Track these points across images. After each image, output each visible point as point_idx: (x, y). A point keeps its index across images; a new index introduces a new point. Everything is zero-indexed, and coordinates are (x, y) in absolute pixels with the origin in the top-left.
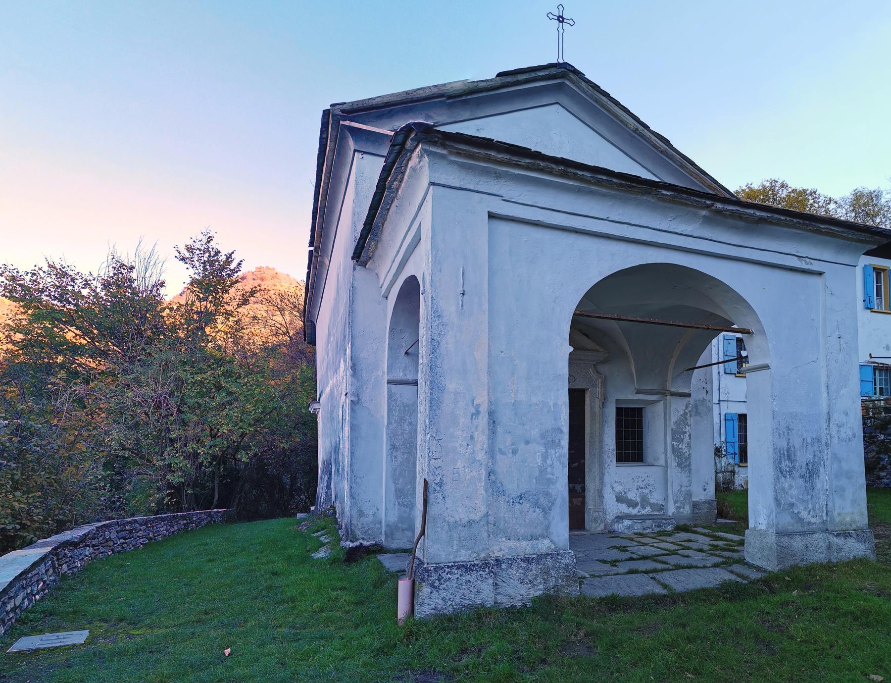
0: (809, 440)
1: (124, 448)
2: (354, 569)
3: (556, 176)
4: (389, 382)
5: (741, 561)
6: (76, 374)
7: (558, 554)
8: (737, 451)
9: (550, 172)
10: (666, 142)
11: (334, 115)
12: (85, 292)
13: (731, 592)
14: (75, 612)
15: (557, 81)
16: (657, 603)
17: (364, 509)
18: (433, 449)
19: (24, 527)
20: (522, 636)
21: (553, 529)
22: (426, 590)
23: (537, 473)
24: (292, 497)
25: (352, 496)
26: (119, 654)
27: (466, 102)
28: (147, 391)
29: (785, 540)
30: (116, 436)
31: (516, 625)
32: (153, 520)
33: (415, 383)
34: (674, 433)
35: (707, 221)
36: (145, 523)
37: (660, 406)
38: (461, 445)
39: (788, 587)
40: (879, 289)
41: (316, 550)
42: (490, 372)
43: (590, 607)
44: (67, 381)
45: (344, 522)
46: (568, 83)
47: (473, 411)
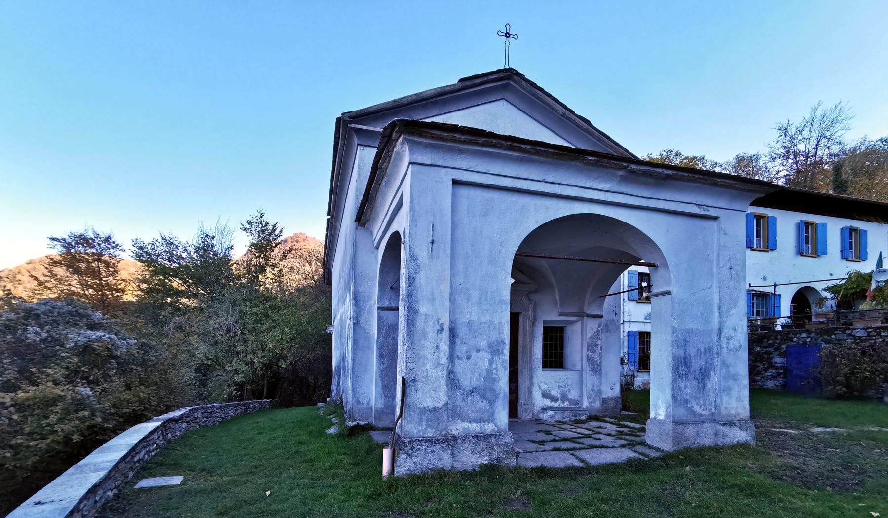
0: (702, 350)
1: (208, 359)
2: (353, 441)
3: (505, 149)
4: (379, 309)
5: (643, 444)
6: (179, 309)
8: (637, 360)
9: (500, 147)
10: (587, 122)
11: (344, 121)
12: (184, 255)
13: (633, 466)
14: (175, 464)
15: (505, 83)
16: (576, 473)
17: (360, 398)
18: (409, 355)
19: (146, 409)
20: (472, 491)
21: (497, 416)
22: (403, 456)
23: (485, 374)
24: (315, 392)
25: (353, 390)
26: (200, 492)
27: (435, 103)
28: (222, 320)
29: (680, 428)
30: (202, 350)
31: (467, 483)
32: (224, 406)
33: (397, 309)
34: (588, 345)
35: (624, 179)
36: (220, 408)
37: (579, 325)
39: (682, 464)
40: (758, 231)
41: (329, 428)
42: (452, 300)
43: (524, 475)
44: (172, 314)
45: (347, 408)
46: (511, 83)
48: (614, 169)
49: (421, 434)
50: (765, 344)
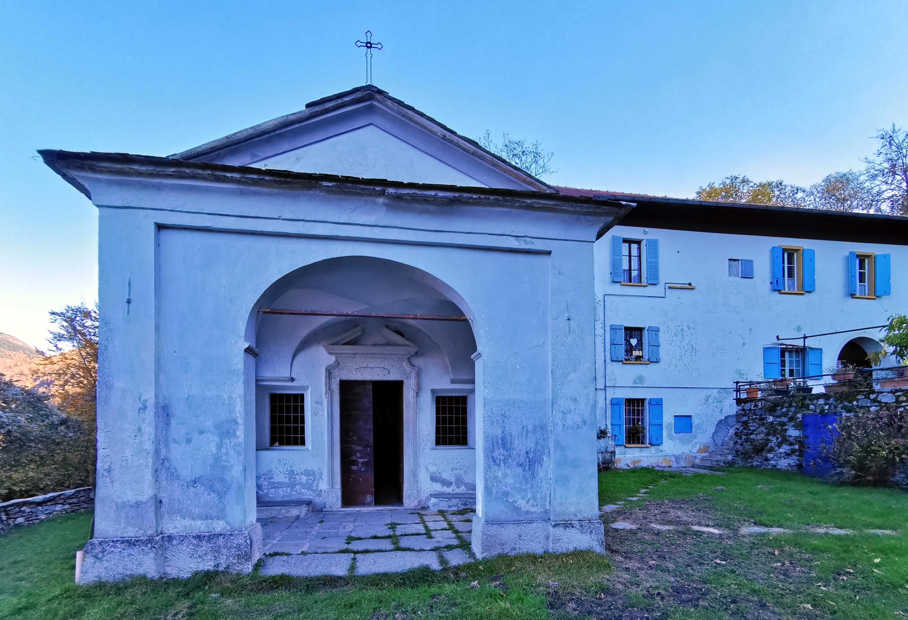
0: (530, 427)
7: (231, 535)
23: (211, 461)
27: (281, 136)
29: (494, 529)
38: (129, 436)
46: (376, 103)
47: (141, 406)
48: (371, 195)
49: (119, 533)
50: (778, 413)
